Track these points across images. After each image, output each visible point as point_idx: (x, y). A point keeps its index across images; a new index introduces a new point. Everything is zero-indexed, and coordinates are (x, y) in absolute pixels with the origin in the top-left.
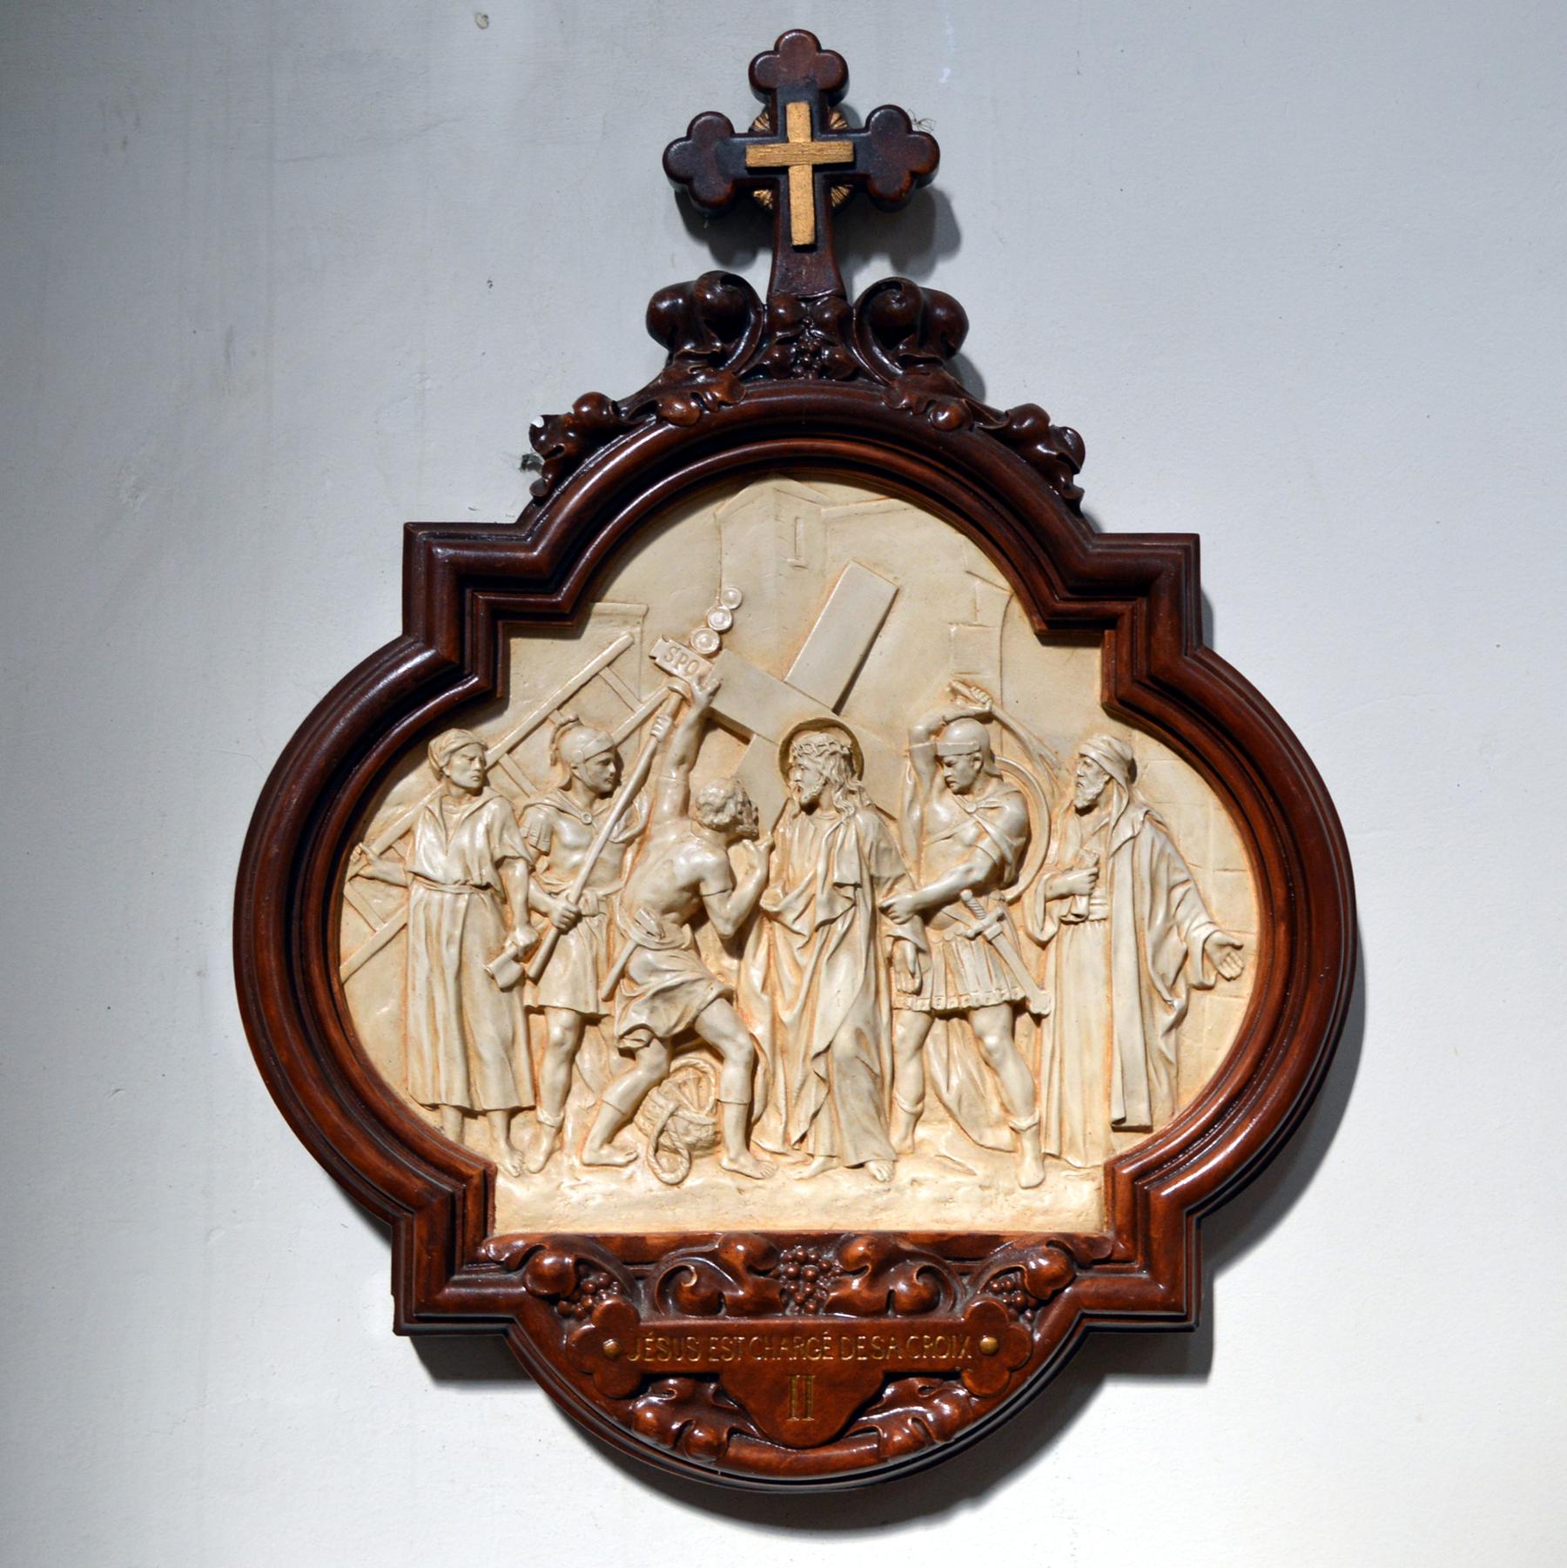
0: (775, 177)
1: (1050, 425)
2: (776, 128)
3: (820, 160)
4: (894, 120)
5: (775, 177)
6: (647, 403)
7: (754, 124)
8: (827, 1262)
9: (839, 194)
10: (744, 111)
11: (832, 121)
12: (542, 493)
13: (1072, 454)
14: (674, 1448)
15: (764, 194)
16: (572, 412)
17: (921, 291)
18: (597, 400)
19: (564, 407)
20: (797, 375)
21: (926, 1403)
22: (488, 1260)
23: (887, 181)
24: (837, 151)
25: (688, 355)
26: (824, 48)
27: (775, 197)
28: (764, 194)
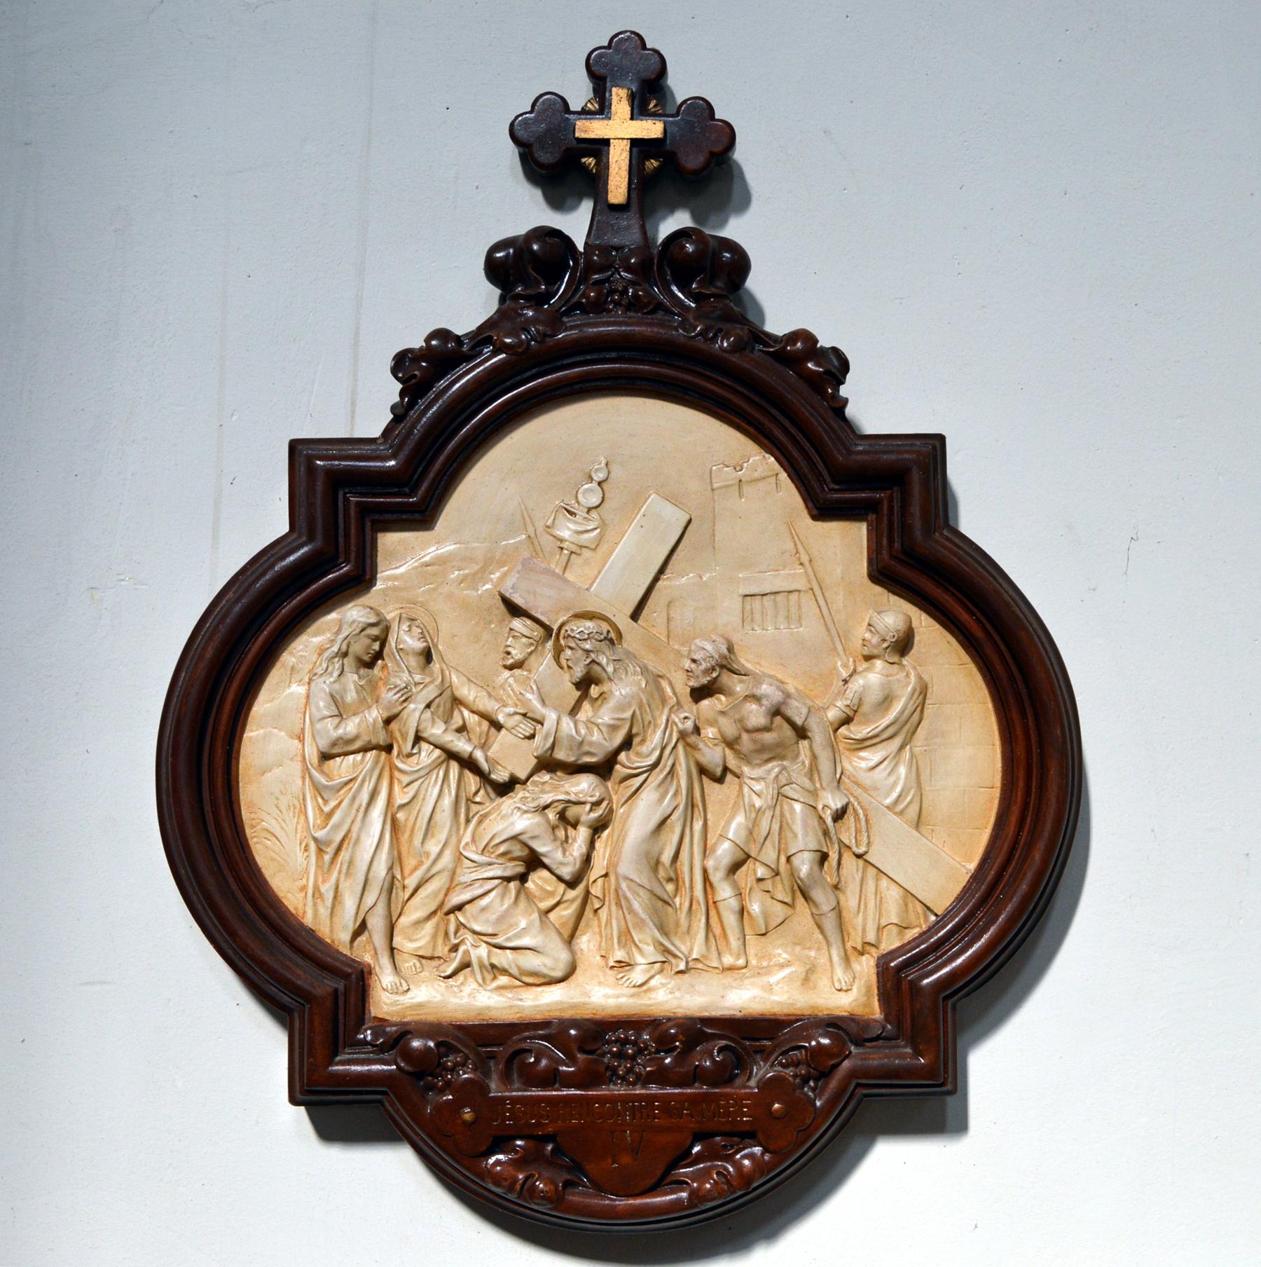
0: (600, 147)
1: (818, 346)
2: (602, 109)
3: (634, 136)
4: (701, 109)
5: (600, 147)
6: (483, 337)
7: (586, 105)
8: (645, 1042)
9: (653, 164)
10: (579, 93)
11: (652, 161)
12: (400, 411)
13: (837, 366)
14: (518, 1198)
15: (590, 161)
16: (424, 345)
17: (710, 240)
18: (443, 334)
19: (417, 343)
20: (610, 311)
21: (729, 1158)
22: (364, 1043)
23: (693, 160)
24: (651, 129)
25: (519, 296)
26: (649, 46)
27: (597, 164)
28: (590, 161)
